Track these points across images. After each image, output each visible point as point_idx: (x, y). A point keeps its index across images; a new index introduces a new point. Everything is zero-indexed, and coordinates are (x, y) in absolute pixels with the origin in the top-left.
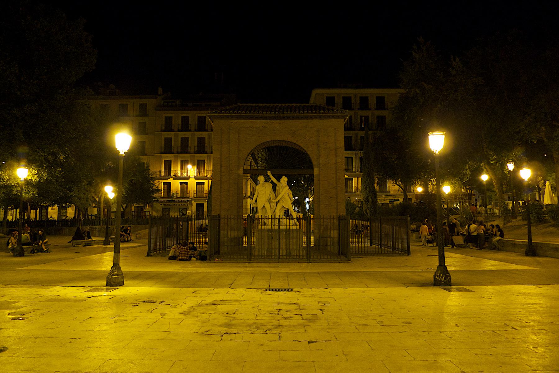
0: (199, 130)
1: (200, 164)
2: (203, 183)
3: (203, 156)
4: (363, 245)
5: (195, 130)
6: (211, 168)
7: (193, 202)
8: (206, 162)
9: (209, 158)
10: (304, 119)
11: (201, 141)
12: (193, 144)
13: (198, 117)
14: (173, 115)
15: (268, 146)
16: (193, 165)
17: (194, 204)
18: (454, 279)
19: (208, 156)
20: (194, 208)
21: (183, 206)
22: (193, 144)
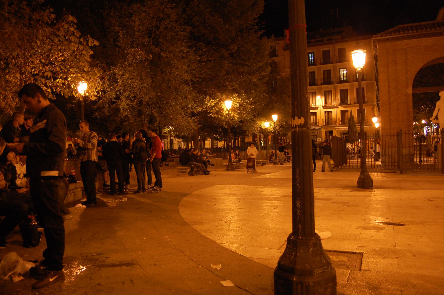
0: (324, 63)
1: (326, 94)
2: (331, 112)
3: (330, 87)
4: (370, 160)
5: (321, 64)
6: (339, 97)
7: (322, 129)
8: (332, 92)
9: (335, 88)
10: (411, 39)
11: (327, 73)
12: (319, 77)
13: (323, 52)
14: (330, 48)
15: (438, 62)
16: (322, 95)
17: (324, 131)
18: (374, 184)
19: (334, 87)
20: (323, 135)
21: (314, 134)
22: (319, 77)
